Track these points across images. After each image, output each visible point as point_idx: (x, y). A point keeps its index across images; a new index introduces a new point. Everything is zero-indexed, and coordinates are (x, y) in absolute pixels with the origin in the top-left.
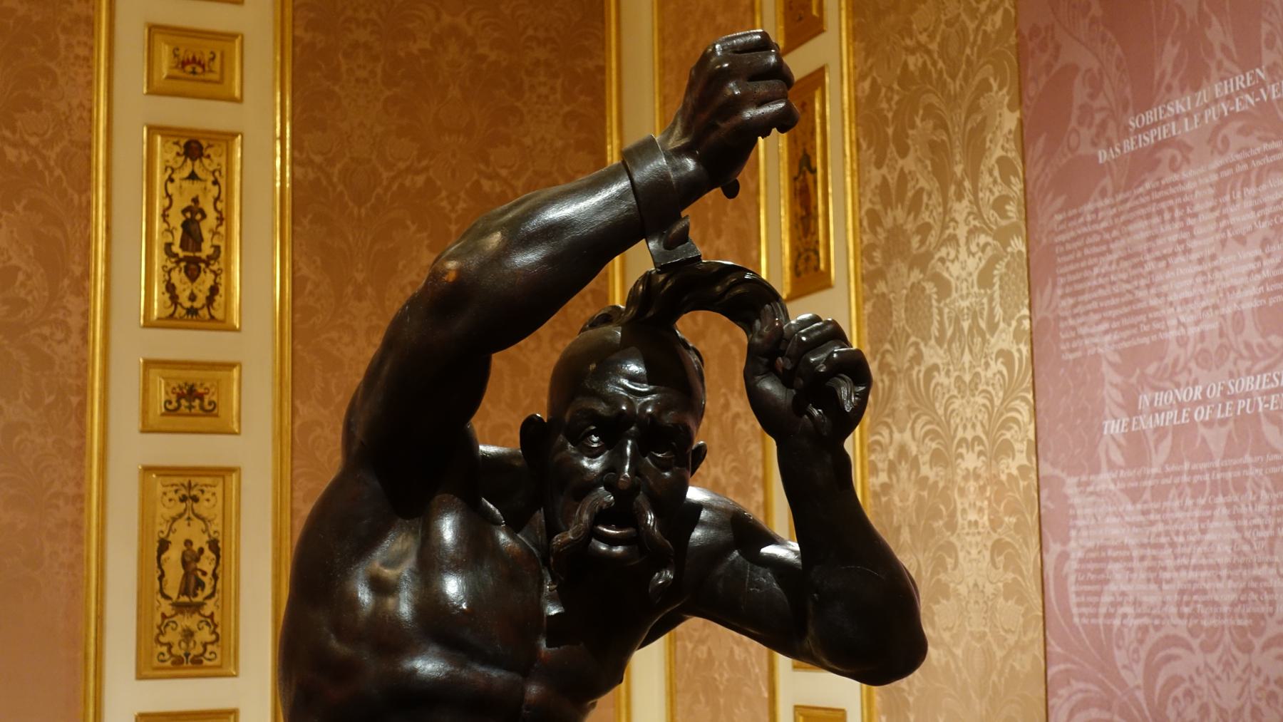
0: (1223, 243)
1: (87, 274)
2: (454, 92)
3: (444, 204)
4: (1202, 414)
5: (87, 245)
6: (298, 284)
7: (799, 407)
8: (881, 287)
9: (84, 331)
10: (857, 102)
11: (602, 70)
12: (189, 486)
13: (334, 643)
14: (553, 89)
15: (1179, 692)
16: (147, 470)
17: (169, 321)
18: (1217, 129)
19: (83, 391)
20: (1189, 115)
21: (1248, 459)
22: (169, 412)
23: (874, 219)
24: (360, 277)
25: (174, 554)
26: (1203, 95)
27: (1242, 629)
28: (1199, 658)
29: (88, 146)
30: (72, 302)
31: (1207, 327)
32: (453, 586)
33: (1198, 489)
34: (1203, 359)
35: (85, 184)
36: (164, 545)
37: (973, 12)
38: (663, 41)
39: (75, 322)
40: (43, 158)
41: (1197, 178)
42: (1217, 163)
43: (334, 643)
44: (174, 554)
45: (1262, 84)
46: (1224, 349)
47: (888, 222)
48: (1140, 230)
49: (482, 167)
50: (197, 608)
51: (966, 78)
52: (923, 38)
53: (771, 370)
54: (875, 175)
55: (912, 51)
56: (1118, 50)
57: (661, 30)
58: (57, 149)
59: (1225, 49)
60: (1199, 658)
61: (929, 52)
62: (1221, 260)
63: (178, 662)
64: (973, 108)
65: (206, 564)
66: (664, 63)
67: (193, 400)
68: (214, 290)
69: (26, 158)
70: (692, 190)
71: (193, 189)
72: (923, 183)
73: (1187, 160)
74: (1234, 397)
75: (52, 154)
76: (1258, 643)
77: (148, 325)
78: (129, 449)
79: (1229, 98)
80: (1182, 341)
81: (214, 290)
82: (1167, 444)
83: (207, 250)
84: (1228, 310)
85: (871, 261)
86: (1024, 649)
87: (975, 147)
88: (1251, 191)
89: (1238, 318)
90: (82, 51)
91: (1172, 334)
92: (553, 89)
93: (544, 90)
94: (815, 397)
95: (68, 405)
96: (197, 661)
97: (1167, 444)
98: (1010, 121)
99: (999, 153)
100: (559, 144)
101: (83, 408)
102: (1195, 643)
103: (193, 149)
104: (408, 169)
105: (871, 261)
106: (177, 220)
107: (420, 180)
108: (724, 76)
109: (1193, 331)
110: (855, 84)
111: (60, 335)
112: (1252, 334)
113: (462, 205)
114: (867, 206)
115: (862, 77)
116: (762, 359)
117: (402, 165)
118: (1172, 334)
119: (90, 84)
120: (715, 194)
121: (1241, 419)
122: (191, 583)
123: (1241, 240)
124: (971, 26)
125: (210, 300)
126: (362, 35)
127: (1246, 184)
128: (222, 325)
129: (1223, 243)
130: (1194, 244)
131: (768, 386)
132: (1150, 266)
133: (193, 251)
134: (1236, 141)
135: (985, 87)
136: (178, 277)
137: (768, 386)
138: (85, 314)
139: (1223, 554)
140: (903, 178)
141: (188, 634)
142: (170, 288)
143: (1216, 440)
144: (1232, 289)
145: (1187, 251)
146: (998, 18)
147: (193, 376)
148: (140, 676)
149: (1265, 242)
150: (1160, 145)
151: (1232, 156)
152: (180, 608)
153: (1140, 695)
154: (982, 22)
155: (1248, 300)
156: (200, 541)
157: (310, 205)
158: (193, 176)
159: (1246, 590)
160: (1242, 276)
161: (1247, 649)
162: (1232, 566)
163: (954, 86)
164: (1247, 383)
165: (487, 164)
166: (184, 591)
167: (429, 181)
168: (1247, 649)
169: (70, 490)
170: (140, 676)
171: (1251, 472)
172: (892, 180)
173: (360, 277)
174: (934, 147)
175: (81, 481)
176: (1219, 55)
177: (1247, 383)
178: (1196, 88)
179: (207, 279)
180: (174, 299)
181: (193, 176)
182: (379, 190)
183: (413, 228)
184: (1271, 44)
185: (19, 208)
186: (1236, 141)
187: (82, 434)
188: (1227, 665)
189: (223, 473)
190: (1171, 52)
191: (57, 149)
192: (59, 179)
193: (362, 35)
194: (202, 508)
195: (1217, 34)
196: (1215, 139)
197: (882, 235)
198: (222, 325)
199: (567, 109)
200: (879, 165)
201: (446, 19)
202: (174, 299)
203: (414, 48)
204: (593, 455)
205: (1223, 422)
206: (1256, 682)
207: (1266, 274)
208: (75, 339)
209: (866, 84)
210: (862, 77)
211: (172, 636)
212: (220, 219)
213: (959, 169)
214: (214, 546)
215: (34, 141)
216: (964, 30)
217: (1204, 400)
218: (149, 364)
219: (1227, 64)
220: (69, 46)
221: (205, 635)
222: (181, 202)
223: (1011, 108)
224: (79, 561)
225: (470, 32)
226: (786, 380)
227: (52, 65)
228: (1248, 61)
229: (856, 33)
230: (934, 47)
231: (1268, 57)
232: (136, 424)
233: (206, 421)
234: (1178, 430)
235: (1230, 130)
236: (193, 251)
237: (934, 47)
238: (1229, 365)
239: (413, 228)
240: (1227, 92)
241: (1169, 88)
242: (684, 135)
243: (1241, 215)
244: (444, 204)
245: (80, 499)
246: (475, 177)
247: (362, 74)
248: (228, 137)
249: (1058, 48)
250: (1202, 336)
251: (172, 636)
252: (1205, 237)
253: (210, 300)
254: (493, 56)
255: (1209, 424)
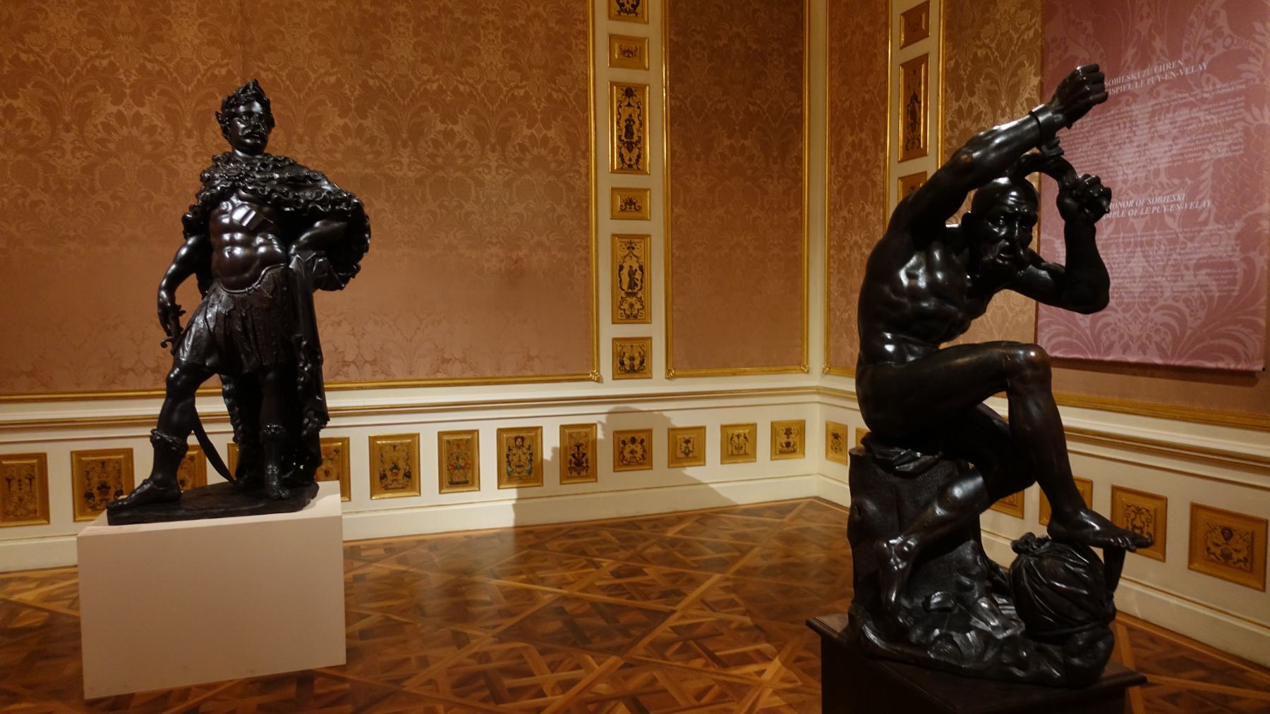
0: (1152, 138)
1: (588, 149)
2: (537, 45)
3: (122, 77)
4: (1134, 212)
5: (587, 135)
6: (673, 154)
7: (1081, 209)
8: (850, 181)
9: (588, 175)
10: (946, 71)
11: (802, 53)
12: (630, 243)
13: (893, 297)
14: (496, 36)
15: (1109, 329)
16: (614, 235)
17: (621, 170)
18: (1154, 87)
19: (588, 201)
20: (1138, 81)
21: (1156, 232)
22: (622, 210)
23: (953, 125)
24: (698, 150)
25: (625, 272)
26: (1147, 72)
27: (1145, 304)
28: (1121, 315)
29: (586, 91)
30: (582, 162)
31: (1139, 175)
32: (939, 276)
33: (1127, 245)
34: (1136, 189)
35: (586, 109)
36: (621, 268)
37: (1016, 30)
38: (831, 38)
39: (583, 170)
40: (43, 59)
41: (1140, 110)
42: (1153, 102)
43: (893, 297)
44: (625, 272)
45: (1180, 67)
46: (1146, 186)
47: (961, 126)
48: (1106, 133)
49: (20, 45)
50: (634, 294)
51: (1011, 60)
52: (987, 41)
53: (1071, 196)
54: (955, 105)
55: (979, 47)
56: (1101, 50)
57: (831, 34)
58: (51, 53)
59: (1162, 51)
60: (1121, 315)
61: (990, 48)
62: (1150, 145)
63: (628, 317)
64: (1014, 75)
65: (638, 276)
66: (831, 49)
67: (631, 205)
68: (639, 156)
69: (157, 68)
70: (1060, 126)
71: (629, 110)
72: (982, 109)
73: (1135, 101)
74: (1151, 206)
75: (571, 95)
76: (1152, 309)
77: (613, 171)
78: (607, 226)
79: (1162, 73)
80: (1125, 182)
81: (639, 156)
82: (1113, 225)
83: (635, 138)
84: (1152, 168)
85: (950, 143)
86: (1024, 313)
87: (1014, 93)
88: (1170, 115)
89: (1157, 173)
90: (582, 47)
91: (1120, 178)
92: (496, 36)
93: (491, 37)
94: (1086, 204)
95: (582, 207)
96: (635, 317)
97: (1113, 225)
98: (1035, 81)
99: (1027, 95)
100: (500, 65)
101: (587, 210)
102: (1119, 309)
103: (629, 92)
104: (97, 56)
105: (950, 143)
106: (623, 124)
107: (522, 92)
108: (1084, 83)
109: (1131, 177)
110: (946, 62)
111: (181, 159)
112: (1163, 178)
113: (133, 78)
114: (949, 119)
115: (950, 59)
116: (1064, 192)
117: (322, 71)
118: (1120, 178)
119: (586, 62)
120: (1065, 129)
121: (1154, 217)
122: (632, 284)
123: (1162, 137)
124: (1015, 36)
125: (637, 161)
126: (491, 17)
127: (1168, 112)
128: (641, 171)
129: (1152, 138)
130: (1136, 139)
131: (1068, 201)
132: (1111, 148)
133: (630, 140)
134: (1164, 93)
135: (1021, 65)
136: (624, 151)
137: (1068, 201)
138: (588, 167)
139: (1138, 272)
140: (971, 106)
141: (632, 306)
142: (621, 155)
143: (1139, 225)
144: (1155, 159)
145: (1131, 142)
146: (1031, 33)
147: (631, 195)
148: (613, 323)
149: (1175, 138)
150: (1120, 94)
151: (1161, 100)
152: (628, 294)
153: (1088, 331)
154: (1023, 33)
155: (1163, 163)
156: (636, 266)
157: (678, 118)
158: (629, 105)
159: (1148, 287)
160: (1162, 154)
161: (1147, 311)
162: (1142, 277)
163: (1003, 64)
164: (1159, 200)
165: (23, 43)
166: (630, 287)
167: (526, 92)
168: (1147, 311)
169: (584, 244)
170: (613, 323)
171: (1157, 238)
172: (857, 141)
173: (493, 140)
174: (990, 92)
175: (588, 240)
176: (1158, 53)
177: (1159, 200)
178: (1144, 68)
179: (636, 151)
180: (623, 160)
181: (629, 105)
182: (78, 68)
183: (101, 91)
184: (1188, 48)
185: (155, 94)
186: (1164, 93)
187: (588, 220)
188: (1136, 318)
189: (643, 237)
190: (1131, 51)
191: (51, 53)
192: (53, 71)
193: (491, 17)
194: (635, 252)
195: (1158, 43)
196: (1152, 92)
197: (957, 132)
198: (641, 171)
199: (201, 21)
200: (957, 100)
201: (735, 29)
202: (623, 160)
203: (721, 44)
204: (1001, 228)
205: (1143, 216)
206: (1149, 325)
207: (1174, 152)
208: (584, 178)
209: (952, 62)
210: (950, 59)
211: (626, 306)
212: (641, 124)
213: (1003, 103)
214: (641, 268)
215: (161, 58)
216: (1011, 39)
217: (1134, 206)
218: (613, 189)
219: (1162, 58)
220: (290, 18)
221: (638, 306)
222: (625, 116)
223: (1035, 75)
224: (589, 274)
225: (545, 15)
226: (1075, 198)
227: (282, 28)
228: (1174, 54)
229: (948, 38)
230: (993, 45)
231: (1185, 55)
232: (609, 215)
233: (638, 214)
234: (1118, 220)
235: (1161, 88)
236: (630, 140)
237: (993, 45)
238: (1150, 191)
239: (101, 91)
240: (1162, 70)
241: (1129, 68)
242: (1061, 104)
243: (1163, 126)
244: (122, 77)
245: (588, 248)
246: (15, 51)
247: (698, 56)
248: (642, 88)
249: (1066, 48)
250: (1136, 179)
251: (626, 306)
252: (1142, 135)
253: (637, 161)
254: (754, 47)
255: (1137, 217)
